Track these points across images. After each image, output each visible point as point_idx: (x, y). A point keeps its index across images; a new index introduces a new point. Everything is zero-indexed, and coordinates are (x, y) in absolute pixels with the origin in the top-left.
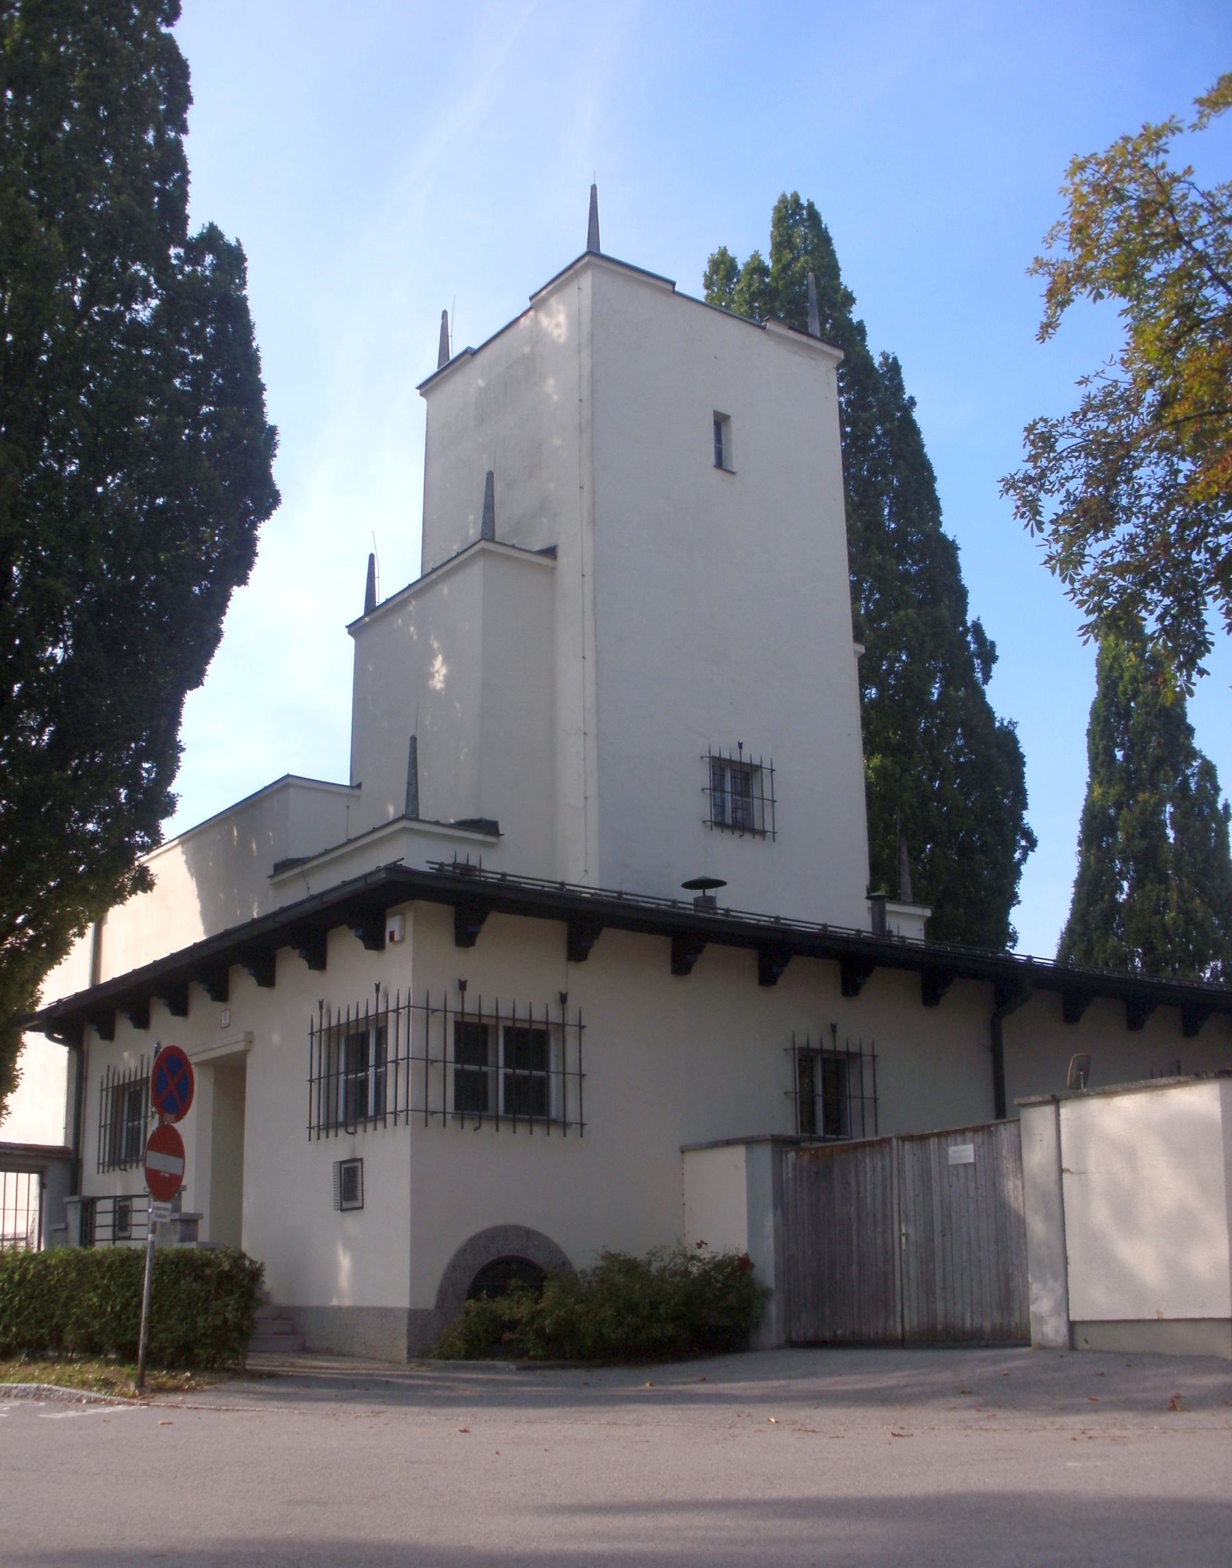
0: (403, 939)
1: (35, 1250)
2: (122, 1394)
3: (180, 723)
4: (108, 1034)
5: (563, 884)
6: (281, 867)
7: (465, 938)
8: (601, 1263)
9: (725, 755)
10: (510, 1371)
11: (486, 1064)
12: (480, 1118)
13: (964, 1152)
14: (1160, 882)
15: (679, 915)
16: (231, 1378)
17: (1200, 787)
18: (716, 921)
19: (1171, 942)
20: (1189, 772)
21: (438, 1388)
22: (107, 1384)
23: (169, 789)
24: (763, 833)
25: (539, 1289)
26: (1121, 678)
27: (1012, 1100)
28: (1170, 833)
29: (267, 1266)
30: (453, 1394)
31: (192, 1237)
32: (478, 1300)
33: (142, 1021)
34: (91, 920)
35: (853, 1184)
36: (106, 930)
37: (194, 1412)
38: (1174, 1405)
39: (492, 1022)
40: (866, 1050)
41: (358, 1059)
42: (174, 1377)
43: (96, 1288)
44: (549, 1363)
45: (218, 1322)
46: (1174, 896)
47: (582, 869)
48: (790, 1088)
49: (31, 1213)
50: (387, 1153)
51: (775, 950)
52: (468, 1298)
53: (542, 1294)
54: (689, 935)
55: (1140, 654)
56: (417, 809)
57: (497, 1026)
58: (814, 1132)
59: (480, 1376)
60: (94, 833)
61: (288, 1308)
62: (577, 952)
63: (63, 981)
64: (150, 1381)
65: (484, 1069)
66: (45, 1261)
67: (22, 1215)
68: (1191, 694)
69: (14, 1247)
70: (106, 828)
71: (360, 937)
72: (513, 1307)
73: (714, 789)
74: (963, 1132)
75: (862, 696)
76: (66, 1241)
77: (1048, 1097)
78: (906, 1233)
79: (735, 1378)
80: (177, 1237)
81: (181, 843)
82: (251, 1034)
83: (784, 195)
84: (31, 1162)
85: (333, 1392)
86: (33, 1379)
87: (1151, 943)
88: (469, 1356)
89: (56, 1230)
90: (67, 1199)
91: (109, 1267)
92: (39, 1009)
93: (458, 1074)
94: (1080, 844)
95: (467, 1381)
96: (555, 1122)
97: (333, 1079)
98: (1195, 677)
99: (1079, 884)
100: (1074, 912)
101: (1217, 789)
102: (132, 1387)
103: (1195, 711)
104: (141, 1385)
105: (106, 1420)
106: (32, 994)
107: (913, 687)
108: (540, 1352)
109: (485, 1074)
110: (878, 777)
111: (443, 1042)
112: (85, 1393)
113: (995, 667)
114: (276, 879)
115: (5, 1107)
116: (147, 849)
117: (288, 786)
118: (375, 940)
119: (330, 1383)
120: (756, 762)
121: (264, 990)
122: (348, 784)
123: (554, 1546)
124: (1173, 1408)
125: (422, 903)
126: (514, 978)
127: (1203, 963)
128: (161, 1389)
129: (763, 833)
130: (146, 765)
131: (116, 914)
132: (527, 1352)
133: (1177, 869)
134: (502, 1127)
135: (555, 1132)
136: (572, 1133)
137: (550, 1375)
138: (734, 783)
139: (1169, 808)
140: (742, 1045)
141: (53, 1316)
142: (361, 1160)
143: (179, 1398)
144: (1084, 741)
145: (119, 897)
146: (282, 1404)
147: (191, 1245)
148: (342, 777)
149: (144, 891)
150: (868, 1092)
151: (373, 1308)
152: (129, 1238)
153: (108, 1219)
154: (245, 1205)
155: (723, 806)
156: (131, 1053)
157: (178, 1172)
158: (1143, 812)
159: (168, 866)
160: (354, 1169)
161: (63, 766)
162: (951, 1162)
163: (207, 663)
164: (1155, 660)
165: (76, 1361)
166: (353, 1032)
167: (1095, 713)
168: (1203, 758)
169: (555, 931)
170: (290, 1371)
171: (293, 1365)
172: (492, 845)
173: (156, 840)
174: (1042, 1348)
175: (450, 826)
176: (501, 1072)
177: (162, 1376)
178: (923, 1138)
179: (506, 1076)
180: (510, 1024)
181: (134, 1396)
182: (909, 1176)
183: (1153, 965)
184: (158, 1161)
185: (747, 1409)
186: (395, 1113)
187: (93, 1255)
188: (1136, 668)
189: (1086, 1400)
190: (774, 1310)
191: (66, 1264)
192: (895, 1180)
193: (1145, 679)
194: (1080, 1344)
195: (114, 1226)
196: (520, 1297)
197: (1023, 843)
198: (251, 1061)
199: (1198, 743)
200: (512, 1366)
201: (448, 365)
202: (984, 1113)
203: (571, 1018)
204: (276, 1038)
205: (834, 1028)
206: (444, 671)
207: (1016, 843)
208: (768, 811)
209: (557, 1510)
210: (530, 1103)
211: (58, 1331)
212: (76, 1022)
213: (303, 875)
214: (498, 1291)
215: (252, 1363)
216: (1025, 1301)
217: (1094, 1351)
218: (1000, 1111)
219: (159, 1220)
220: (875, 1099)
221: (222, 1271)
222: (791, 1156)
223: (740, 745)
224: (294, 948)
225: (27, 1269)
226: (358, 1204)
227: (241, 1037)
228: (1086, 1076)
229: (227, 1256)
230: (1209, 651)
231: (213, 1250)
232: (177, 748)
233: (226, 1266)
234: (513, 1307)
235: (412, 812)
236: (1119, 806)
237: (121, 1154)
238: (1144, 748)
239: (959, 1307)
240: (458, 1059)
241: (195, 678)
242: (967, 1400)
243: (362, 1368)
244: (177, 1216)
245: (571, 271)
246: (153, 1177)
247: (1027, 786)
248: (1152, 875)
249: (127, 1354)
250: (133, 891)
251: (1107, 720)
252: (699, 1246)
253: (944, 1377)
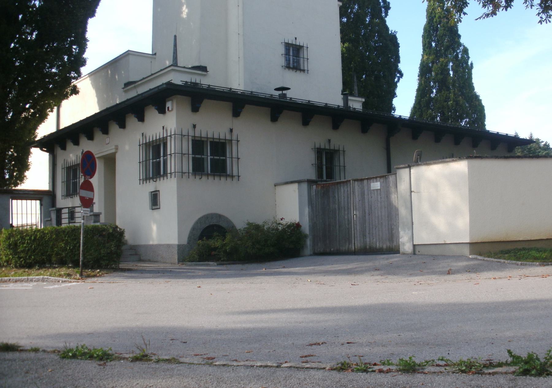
0: (172, 110)
1: (39, 228)
2: (74, 279)
3: (87, 31)
4: (64, 148)
5: (231, 89)
6: (127, 84)
7: (195, 109)
8: (246, 226)
10: (215, 266)
11: (203, 155)
12: (202, 175)
13: (376, 185)
14: (447, 91)
15: (273, 100)
16: (114, 271)
17: (462, 57)
18: (288, 102)
19: (451, 112)
20: (458, 51)
21: (189, 272)
22: (69, 275)
23: (84, 56)
24: (304, 71)
25: (224, 236)
26: (435, 16)
27: (394, 167)
28: (451, 73)
29: (126, 230)
30: (194, 274)
31: (98, 221)
32: (203, 240)
33: (77, 143)
34: (55, 105)
35: (337, 197)
36: (62, 109)
37: (101, 284)
38: (449, 273)
39: (205, 139)
40: (341, 149)
41: (157, 154)
42: (93, 272)
43: (63, 240)
45: (109, 251)
46: (452, 95)
47: (238, 83)
48: (314, 162)
49: (37, 215)
50: (168, 187)
51: (308, 113)
52: (199, 240)
53: (225, 238)
54: (278, 108)
55: (442, 8)
56: (177, 62)
57: (207, 141)
58: (322, 178)
59: (204, 268)
60: (55, 73)
61: (134, 246)
62: (236, 114)
63: (45, 129)
64: (84, 274)
65: (203, 156)
66: (43, 232)
67: (34, 216)
68: (461, 21)
69: (32, 227)
70: (60, 71)
71: (157, 109)
72: (216, 243)
73: (286, 54)
74: (376, 178)
75: (341, 22)
76: (51, 224)
77: (407, 165)
78: (356, 214)
79: (296, 267)
80: (93, 221)
81: (89, 76)
84: (36, 196)
85: (152, 275)
86: (41, 274)
87: (443, 112)
89: (47, 221)
90: (51, 209)
91: (68, 233)
92: (37, 139)
93: (193, 158)
94: (419, 76)
95: (199, 269)
96: (229, 175)
97: (148, 162)
98: (462, 15)
99: (418, 90)
100: (416, 101)
101: (469, 58)
102: (78, 276)
103: (462, 29)
104: (81, 275)
105: (69, 288)
106: (34, 134)
107: (359, 18)
108: (225, 258)
109: (203, 158)
110: (346, 50)
111: (188, 147)
112: (61, 279)
113: (389, 11)
115: (25, 176)
116: (76, 78)
117: (129, 54)
118: (162, 110)
119: (150, 272)
120: (301, 44)
121: (122, 130)
122: (151, 53)
123: (233, 326)
124: (449, 273)
125: (179, 96)
126: (213, 124)
127: (462, 119)
128: (89, 276)
129: (304, 71)
130: (74, 47)
131: (65, 103)
132: (221, 258)
133: (454, 86)
134: (210, 178)
135: (229, 179)
136: (235, 179)
137: (229, 266)
138: (293, 53)
139: (451, 64)
140: (296, 148)
141: (47, 252)
142: (159, 191)
143: (95, 279)
144: (421, 39)
145: (66, 97)
146: (133, 280)
147: (98, 224)
148: (148, 50)
149: (76, 94)
150: (342, 164)
152: (75, 222)
153: (66, 216)
154: (117, 209)
155: (289, 60)
156: (72, 155)
157: (91, 197)
158: (441, 65)
159: (84, 84)
161: (42, 47)
162: (372, 189)
163: (96, 8)
164: (448, 10)
165: (57, 268)
166: (155, 144)
167: (425, 29)
168: (464, 46)
169: (228, 106)
170: (136, 268)
171: (136, 266)
172: (205, 75)
173: (79, 75)
174: (404, 254)
175: (189, 68)
176: (209, 158)
177: (89, 271)
178: (362, 180)
179: (211, 159)
180: (212, 140)
181: (79, 279)
182: (357, 194)
183: (444, 118)
184: (84, 193)
185: (299, 277)
186: (171, 173)
187: (61, 229)
188: (441, 13)
189: (419, 272)
190: (309, 242)
191: (51, 232)
192: (352, 195)
193: (444, 17)
194: (417, 253)
195: (69, 218)
196: (218, 239)
197: (398, 75)
198: (118, 157)
199: (462, 41)
200: (215, 264)
202: (384, 172)
203: (234, 138)
204: (127, 147)
205: (329, 141)
206: (187, 11)
207: (396, 75)
209: (233, 313)
210: (220, 169)
211: (50, 256)
212: (50, 144)
213: (135, 87)
214: (209, 237)
215: (122, 266)
216: (398, 238)
217: (422, 255)
218: (389, 171)
219: (85, 215)
220: (344, 167)
221: (109, 233)
222: (314, 187)
223: (296, 39)
224: (132, 114)
225: (36, 235)
226: (158, 207)
227: (114, 147)
228: (420, 158)
229: (111, 227)
230: (467, 6)
231: (106, 225)
232: (86, 40)
233: (111, 231)
234: (216, 243)
235: (175, 63)
236: (433, 63)
237: (70, 193)
238: (443, 42)
239: (374, 240)
240: (193, 153)
241: (92, 14)
242: (378, 272)
243: (162, 266)
244: (92, 213)
246: (82, 199)
247: (400, 55)
248: (444, 88)
249: (76, 264)
250: (71, 94)
251: (429, 31)
252: (282, 219)
253: (370, 264)
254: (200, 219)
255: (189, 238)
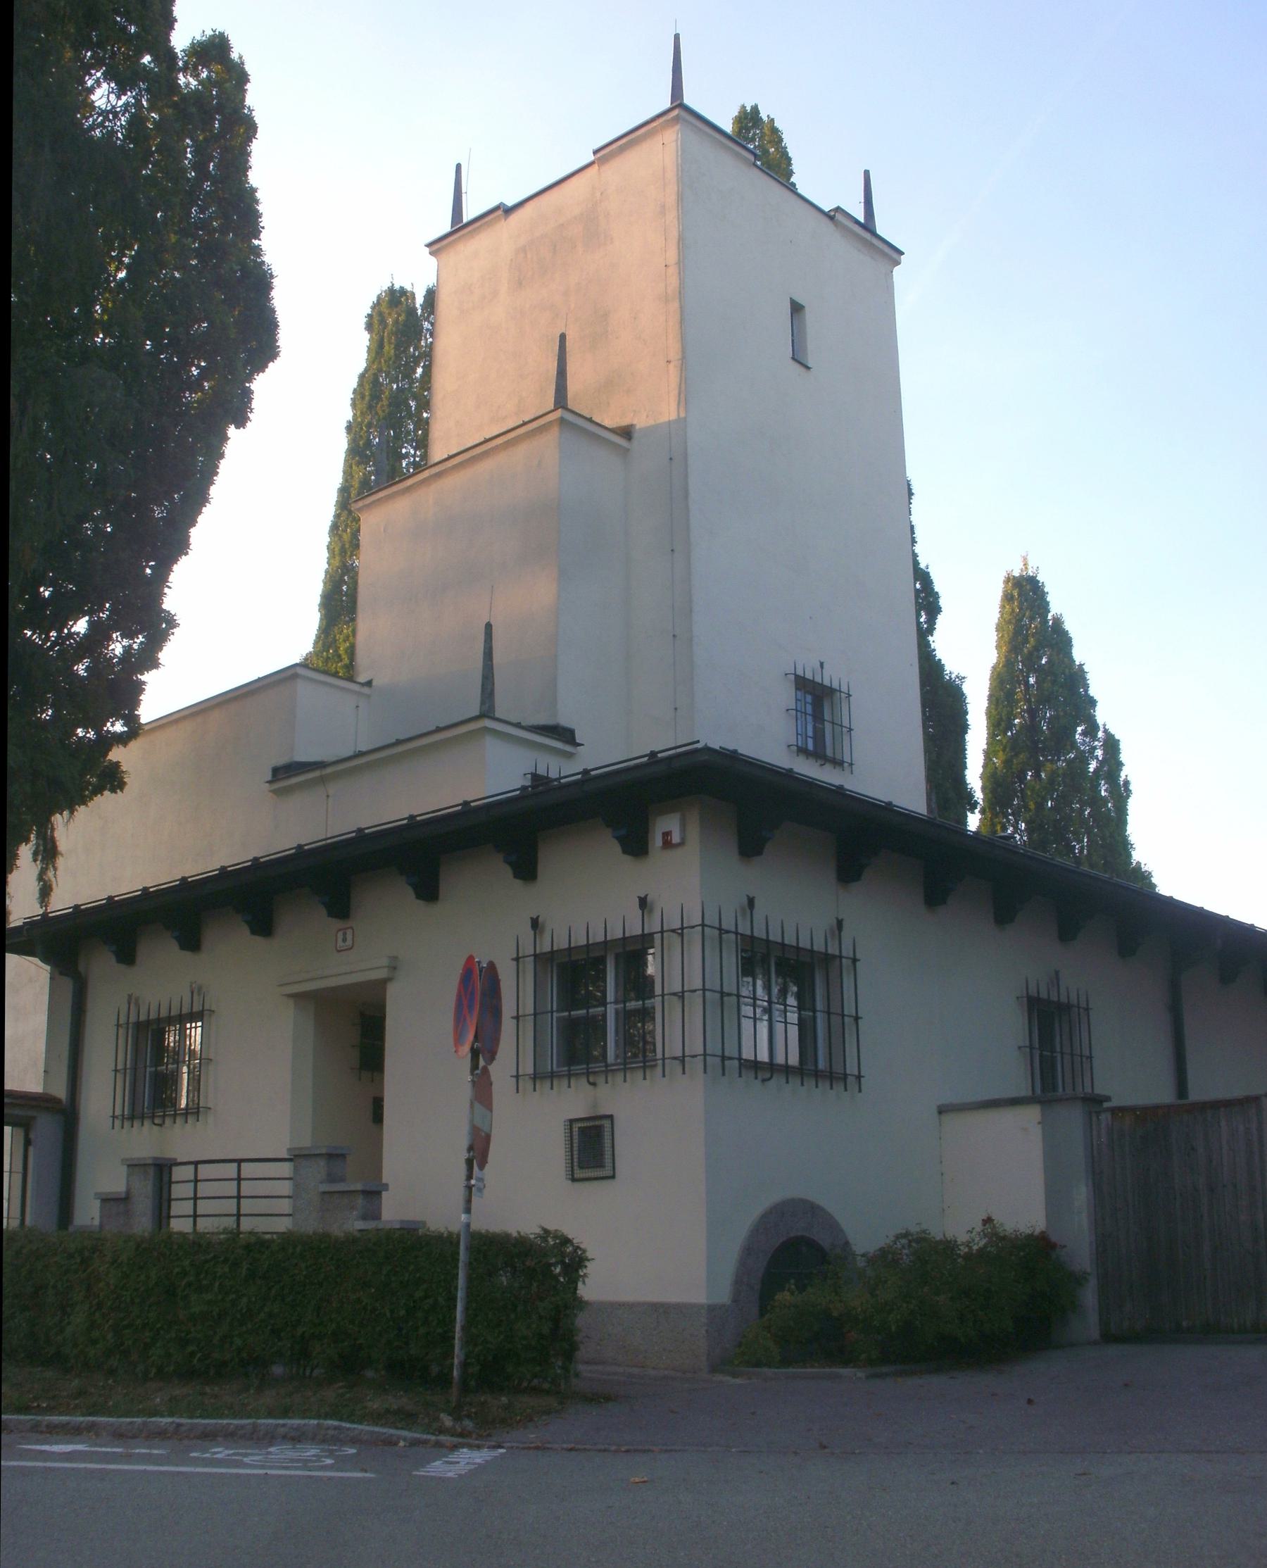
6: (283, 772)
9: (809, 676)
44: (884, 1369)
58: (1055, 1089)
82: (395, 958)
83: (743, 107)
88: (786, 1362)
114: (276, 786)
120: (835, 685)
142: (611, 1117)
149: (113, 790)
151: (639, 1304)
160: (598, 1131)
190: (1089, 1296)
201: (460, 226)
208: (846, 738)
213: (323, 780)
223: (822, 664)
227: (385, 962)
235: (487, 712)
245: (664, 118)
250: (98, 790)
254: (765, 1216)
255: (738, 1282)
